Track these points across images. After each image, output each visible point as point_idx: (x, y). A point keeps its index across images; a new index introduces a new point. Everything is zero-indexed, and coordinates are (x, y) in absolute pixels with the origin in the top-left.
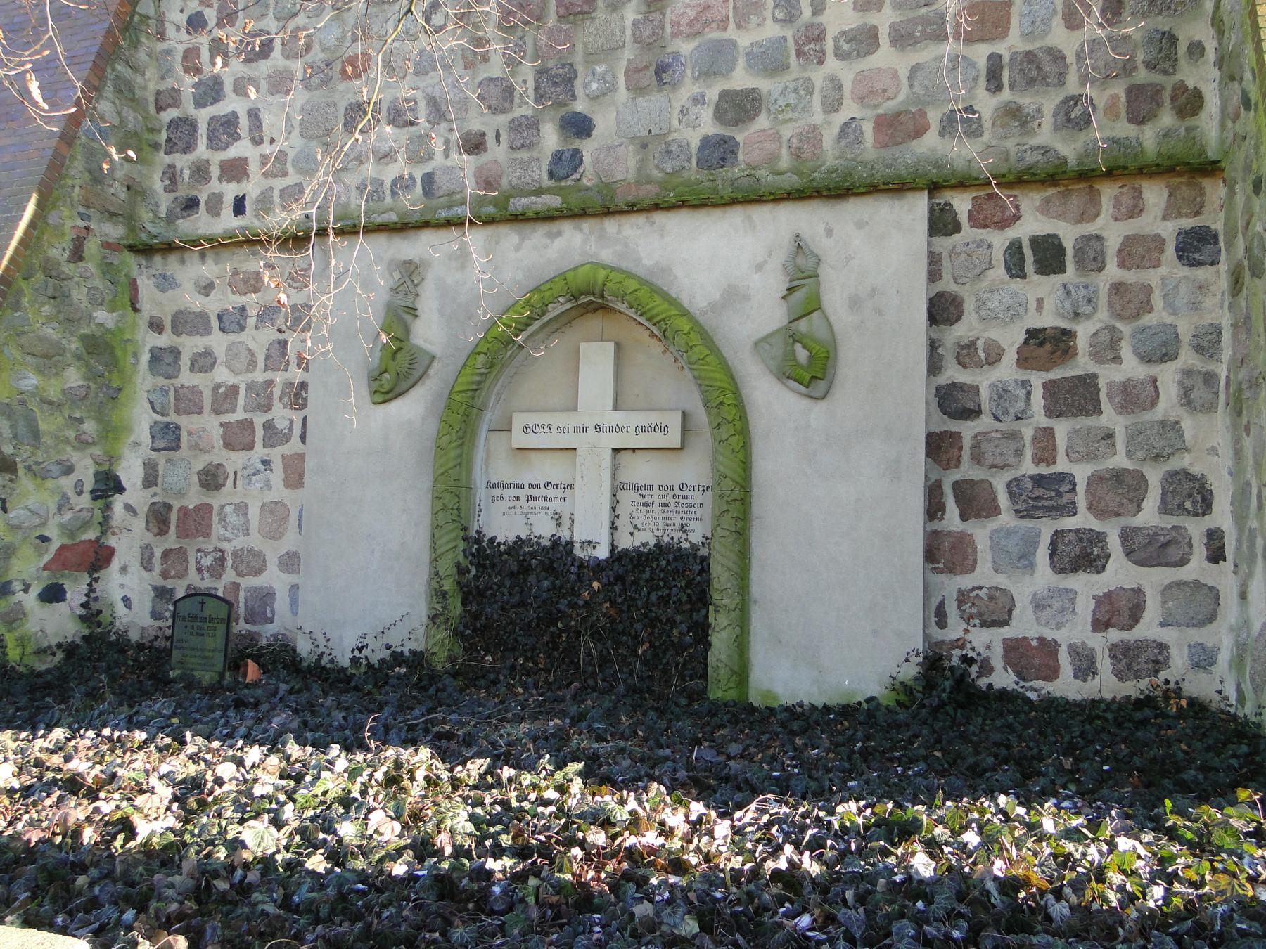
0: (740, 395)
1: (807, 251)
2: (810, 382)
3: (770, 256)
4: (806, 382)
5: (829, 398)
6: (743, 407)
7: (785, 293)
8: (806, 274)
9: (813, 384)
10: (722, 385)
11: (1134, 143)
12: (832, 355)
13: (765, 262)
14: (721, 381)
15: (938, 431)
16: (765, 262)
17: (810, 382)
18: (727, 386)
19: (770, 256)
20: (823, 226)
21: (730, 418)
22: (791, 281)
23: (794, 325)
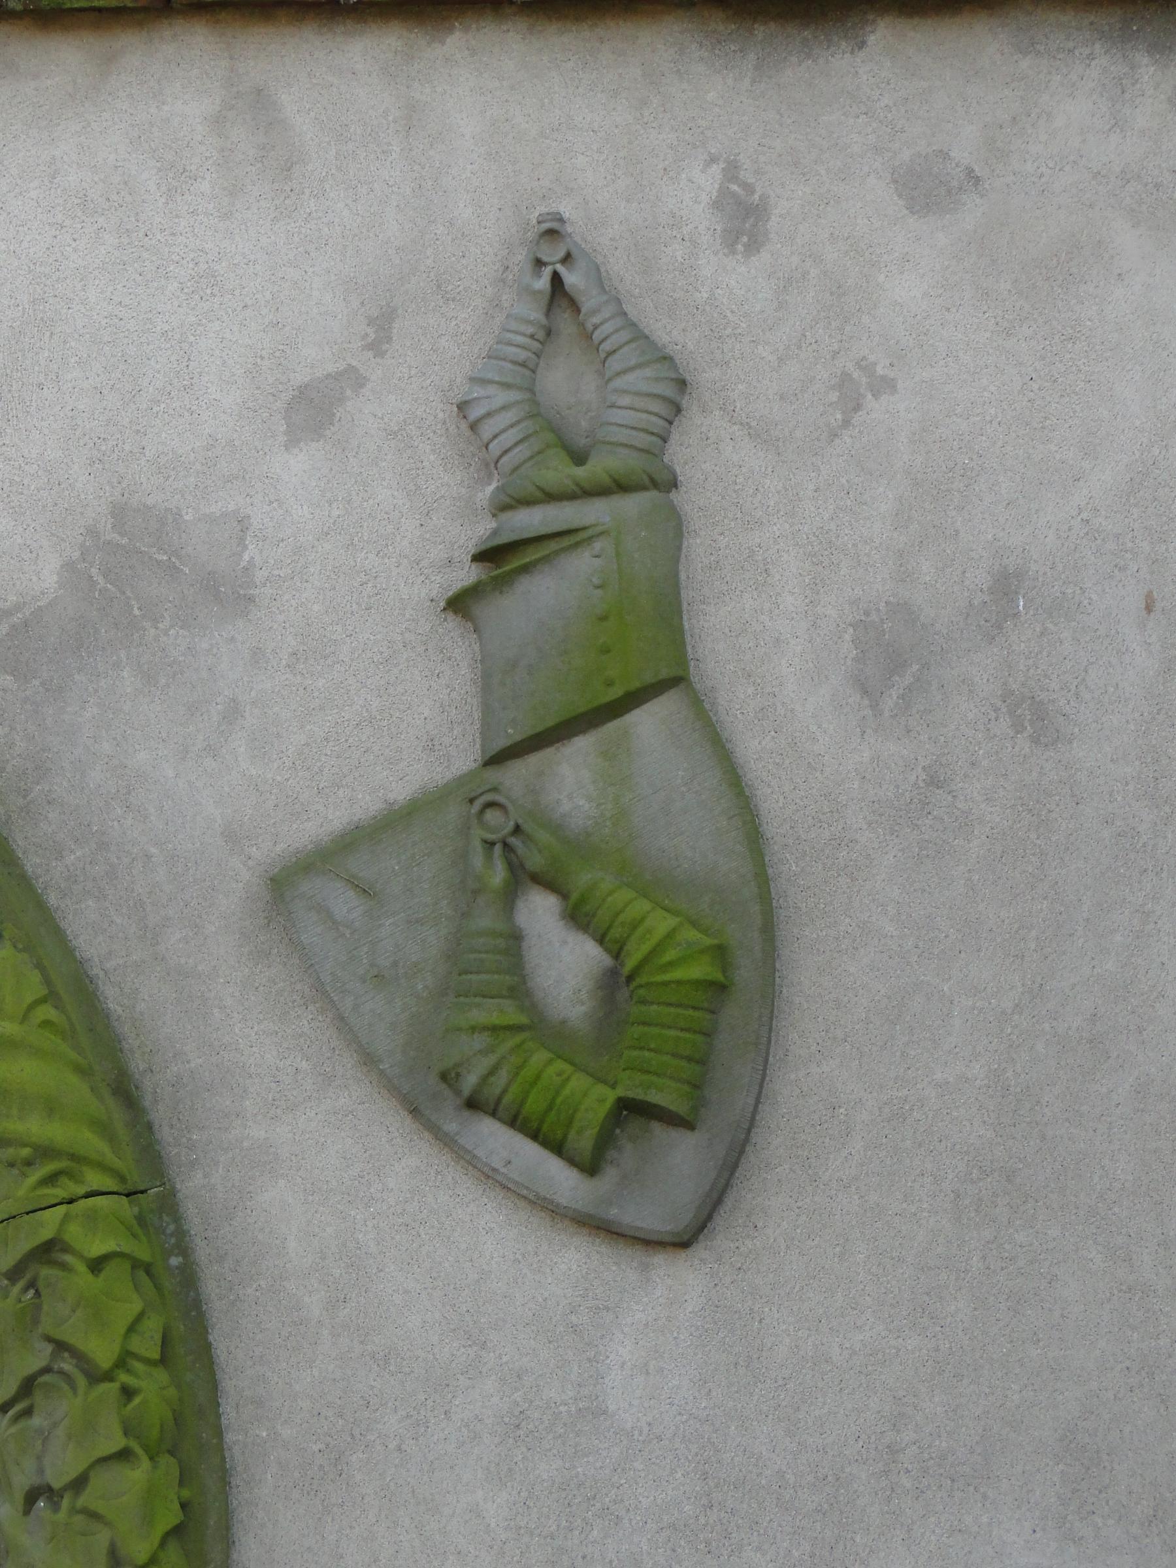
0: (169, 1204)
1: (608, 330)
2: (605, 1141)
3: (376, 347)
4: (583, 1141)
5: (699, 1251)
6: (189, 1278)
7: (467, 575)
8: (598, 468)
9: (627, 1154)
10: (56, 1132)
11: (574, 488)
12: (745, 972)
13: (352, 378)
14: (51, 1108)
15: (640, 1226)
16: (352, 378)
17: (605, 1141)
18: (91, 1142)
19: (376, 347)
20: (708, 181)
21: (103, 1353)
22: (506, 504)
23: (494, 775)
